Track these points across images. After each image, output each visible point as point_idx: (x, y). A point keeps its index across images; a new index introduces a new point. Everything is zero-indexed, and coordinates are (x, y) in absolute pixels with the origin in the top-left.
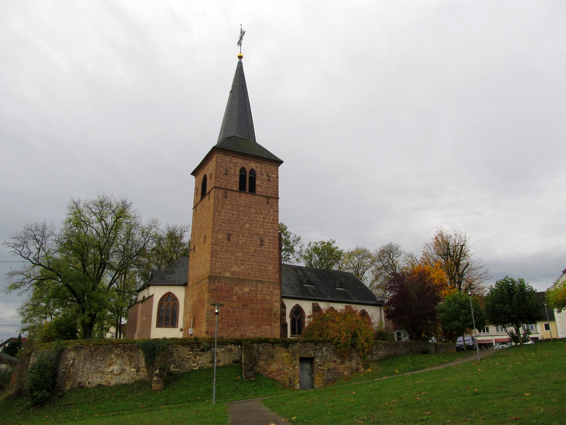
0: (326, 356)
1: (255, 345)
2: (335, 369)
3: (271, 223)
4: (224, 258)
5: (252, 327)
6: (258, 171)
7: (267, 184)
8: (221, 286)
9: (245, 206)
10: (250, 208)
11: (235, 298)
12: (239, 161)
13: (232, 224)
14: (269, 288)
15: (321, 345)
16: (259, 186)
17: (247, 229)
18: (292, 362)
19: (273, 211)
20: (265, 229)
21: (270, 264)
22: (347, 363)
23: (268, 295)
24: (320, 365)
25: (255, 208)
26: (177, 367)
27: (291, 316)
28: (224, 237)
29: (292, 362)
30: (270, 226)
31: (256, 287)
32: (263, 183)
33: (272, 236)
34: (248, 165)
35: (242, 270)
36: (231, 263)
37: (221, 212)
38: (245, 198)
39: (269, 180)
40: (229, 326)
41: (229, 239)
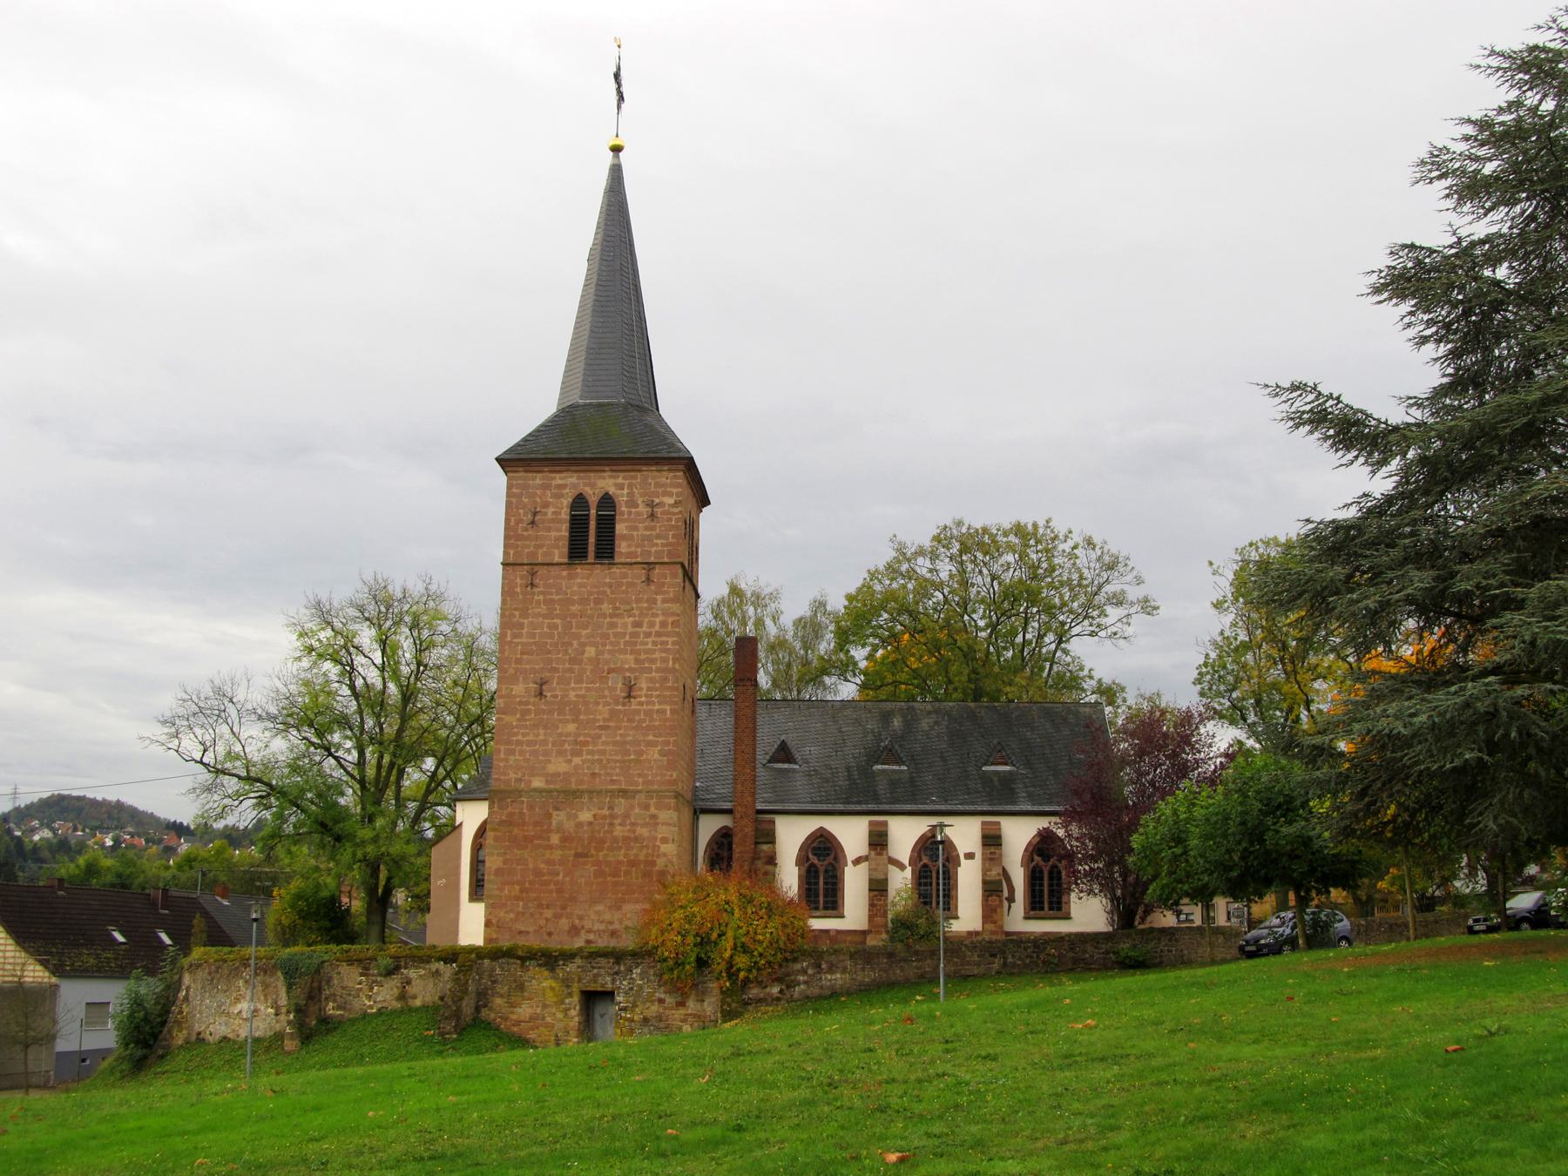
0: (641, 987)
1: (486, 962)
2: (659, 1018)
3: (658, 634)
4: (529, 743)
5: (600, 908)
6: (622, 497)
7: (646, 529)
8: (521, 814)
9: (583, 601)
10: (598, 602)
11: (555, 839)
12: (570, 480)
13: (549, 652)
14: (647, 807)
15: (628, 962)
16: (624, 537)
17: (590, 659)
18: (562, 1002)
19: (664, 601)
20: (638, 652)
21: (650, 744)
22: (692, 1005)
23: (644, 825)
24: (625, 1009)
25: (612, 602)
26: (339, 1008)
27: (802, 859)
28: (527, 690)
29: (562, 1002)
30: (655, 643)
31: (611, 808)
32: (636, 529)
33: (658, 670)
34: (593, 486)
35: (576, 767)
36: (546, 753)
37: (521, 626)
38: (588, 578)
39: (652, 516)
40: (540, 906)
41: (541, 694)
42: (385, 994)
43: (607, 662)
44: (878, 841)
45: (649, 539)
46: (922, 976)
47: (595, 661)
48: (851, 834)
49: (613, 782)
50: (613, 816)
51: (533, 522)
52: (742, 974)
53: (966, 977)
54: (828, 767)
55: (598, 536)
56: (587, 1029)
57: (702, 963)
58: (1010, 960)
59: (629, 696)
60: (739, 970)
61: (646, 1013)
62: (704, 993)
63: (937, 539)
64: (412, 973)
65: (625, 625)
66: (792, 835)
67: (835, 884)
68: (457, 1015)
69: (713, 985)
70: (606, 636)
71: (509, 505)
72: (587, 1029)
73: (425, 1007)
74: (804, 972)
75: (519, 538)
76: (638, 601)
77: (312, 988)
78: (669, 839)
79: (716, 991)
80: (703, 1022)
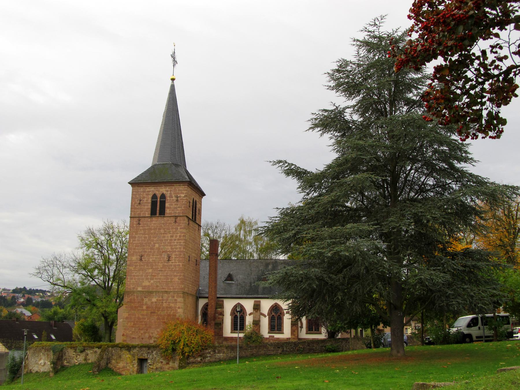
0: (156, 358)
1: (110, 348)
2: (161, 368)
3: (178, 240)
4: (137, 276)
6: (168, 194)
7: (175, 205)
8: (134, 299)
9: (155, 229)
10: (160, 229)
11: (145, 307)
14: (173, 297)
16: (168, 208)
17: (157, 248)
18: (132, 362)
19: (181, 228)
20: (172, 246)
22: (171, 364)
23: (173, 303)
24: (150, 365)
25: (164, 229)
26: (67, 363)
29: (132, 362)
30: (177, 243)
31: (162, 297)
32: (172, 205)
33: (178, 251)
34: (159, 191)
35: (152, 284)
37: (135, 237)
38: (157, 221)
40: (139, 329)
42: (81, 358)
43: (162, 249)
44: (257, 307)
45: (176, 208)
46: (252, 355)
47: (158, 249)
48: (248, 305)
49: (163, 288)
50: (163, 300)
51: (140, 203)
52: (187, 354)
53: (268, 355)
54: (244, 282)
55: (160, 208)
56: (140, 370)
57: (174, 350)
58: (285, 349)
59: (169, 260)
60: (186, 352)
61: (157, 366)
62: (175, 360)
64: (89, 352)
65: (168, 237)
66: (229, 305)
67: (243, 322)
68: (99, 366)
69: (177, 357)
70: (162, 240)
71: (132, 198)
72: (140, 370)
73: (92, 363)
74: (209, 353)
75: (135, 208)
76: (172, 229)
77: (59, 356)
78: (180, 308)
79: (178, 359)
80: (173, 368)
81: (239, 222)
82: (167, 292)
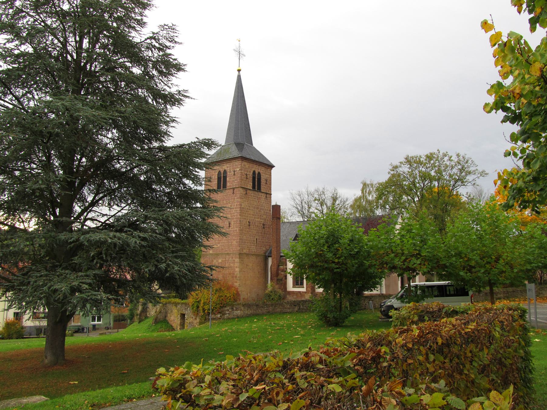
3: (236, 208)
6: (261, 172)
10: (223, 201)
14: (233, 258)
21: (234, 240)
34: (222, 168)
45: (234, 181)
46: (269, 312)
58: (301, 307)
63: (427, 156)
74: (228, 310)
81: (362, 185)
82: (228, 253)
